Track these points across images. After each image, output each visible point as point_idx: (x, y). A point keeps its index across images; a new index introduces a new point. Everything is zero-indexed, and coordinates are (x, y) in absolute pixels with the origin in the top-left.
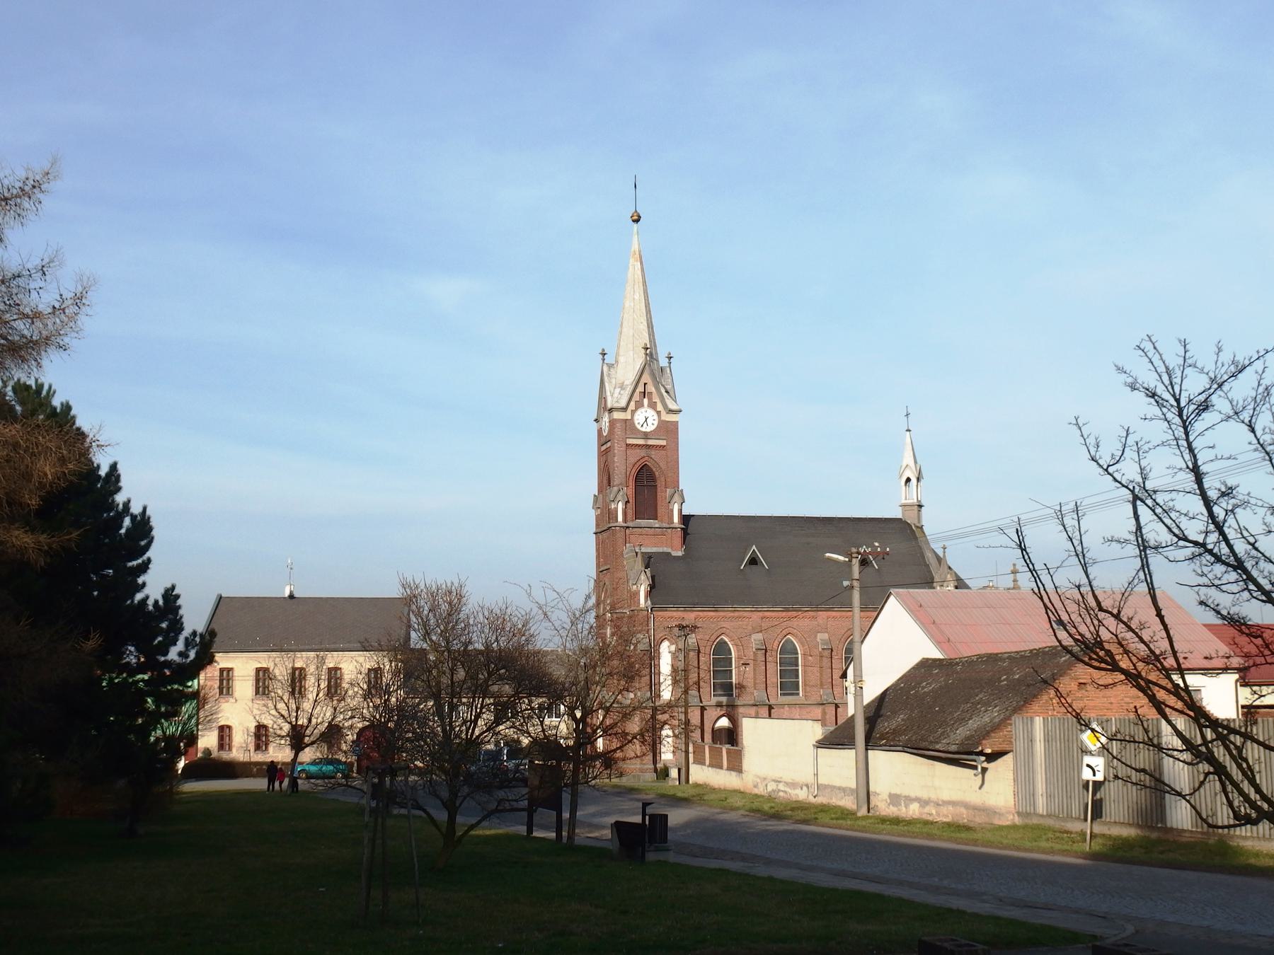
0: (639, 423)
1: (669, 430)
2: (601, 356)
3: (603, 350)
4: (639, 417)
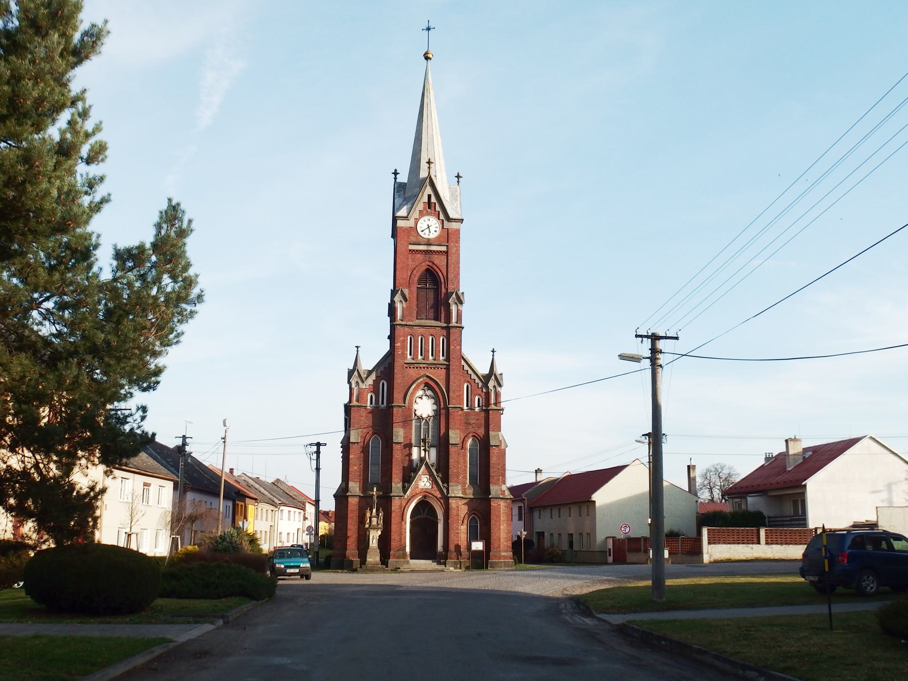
0: (421, 227)
1: (450, 238)
2: (393, 175)
3: (396, 170)
4: (422, 224)
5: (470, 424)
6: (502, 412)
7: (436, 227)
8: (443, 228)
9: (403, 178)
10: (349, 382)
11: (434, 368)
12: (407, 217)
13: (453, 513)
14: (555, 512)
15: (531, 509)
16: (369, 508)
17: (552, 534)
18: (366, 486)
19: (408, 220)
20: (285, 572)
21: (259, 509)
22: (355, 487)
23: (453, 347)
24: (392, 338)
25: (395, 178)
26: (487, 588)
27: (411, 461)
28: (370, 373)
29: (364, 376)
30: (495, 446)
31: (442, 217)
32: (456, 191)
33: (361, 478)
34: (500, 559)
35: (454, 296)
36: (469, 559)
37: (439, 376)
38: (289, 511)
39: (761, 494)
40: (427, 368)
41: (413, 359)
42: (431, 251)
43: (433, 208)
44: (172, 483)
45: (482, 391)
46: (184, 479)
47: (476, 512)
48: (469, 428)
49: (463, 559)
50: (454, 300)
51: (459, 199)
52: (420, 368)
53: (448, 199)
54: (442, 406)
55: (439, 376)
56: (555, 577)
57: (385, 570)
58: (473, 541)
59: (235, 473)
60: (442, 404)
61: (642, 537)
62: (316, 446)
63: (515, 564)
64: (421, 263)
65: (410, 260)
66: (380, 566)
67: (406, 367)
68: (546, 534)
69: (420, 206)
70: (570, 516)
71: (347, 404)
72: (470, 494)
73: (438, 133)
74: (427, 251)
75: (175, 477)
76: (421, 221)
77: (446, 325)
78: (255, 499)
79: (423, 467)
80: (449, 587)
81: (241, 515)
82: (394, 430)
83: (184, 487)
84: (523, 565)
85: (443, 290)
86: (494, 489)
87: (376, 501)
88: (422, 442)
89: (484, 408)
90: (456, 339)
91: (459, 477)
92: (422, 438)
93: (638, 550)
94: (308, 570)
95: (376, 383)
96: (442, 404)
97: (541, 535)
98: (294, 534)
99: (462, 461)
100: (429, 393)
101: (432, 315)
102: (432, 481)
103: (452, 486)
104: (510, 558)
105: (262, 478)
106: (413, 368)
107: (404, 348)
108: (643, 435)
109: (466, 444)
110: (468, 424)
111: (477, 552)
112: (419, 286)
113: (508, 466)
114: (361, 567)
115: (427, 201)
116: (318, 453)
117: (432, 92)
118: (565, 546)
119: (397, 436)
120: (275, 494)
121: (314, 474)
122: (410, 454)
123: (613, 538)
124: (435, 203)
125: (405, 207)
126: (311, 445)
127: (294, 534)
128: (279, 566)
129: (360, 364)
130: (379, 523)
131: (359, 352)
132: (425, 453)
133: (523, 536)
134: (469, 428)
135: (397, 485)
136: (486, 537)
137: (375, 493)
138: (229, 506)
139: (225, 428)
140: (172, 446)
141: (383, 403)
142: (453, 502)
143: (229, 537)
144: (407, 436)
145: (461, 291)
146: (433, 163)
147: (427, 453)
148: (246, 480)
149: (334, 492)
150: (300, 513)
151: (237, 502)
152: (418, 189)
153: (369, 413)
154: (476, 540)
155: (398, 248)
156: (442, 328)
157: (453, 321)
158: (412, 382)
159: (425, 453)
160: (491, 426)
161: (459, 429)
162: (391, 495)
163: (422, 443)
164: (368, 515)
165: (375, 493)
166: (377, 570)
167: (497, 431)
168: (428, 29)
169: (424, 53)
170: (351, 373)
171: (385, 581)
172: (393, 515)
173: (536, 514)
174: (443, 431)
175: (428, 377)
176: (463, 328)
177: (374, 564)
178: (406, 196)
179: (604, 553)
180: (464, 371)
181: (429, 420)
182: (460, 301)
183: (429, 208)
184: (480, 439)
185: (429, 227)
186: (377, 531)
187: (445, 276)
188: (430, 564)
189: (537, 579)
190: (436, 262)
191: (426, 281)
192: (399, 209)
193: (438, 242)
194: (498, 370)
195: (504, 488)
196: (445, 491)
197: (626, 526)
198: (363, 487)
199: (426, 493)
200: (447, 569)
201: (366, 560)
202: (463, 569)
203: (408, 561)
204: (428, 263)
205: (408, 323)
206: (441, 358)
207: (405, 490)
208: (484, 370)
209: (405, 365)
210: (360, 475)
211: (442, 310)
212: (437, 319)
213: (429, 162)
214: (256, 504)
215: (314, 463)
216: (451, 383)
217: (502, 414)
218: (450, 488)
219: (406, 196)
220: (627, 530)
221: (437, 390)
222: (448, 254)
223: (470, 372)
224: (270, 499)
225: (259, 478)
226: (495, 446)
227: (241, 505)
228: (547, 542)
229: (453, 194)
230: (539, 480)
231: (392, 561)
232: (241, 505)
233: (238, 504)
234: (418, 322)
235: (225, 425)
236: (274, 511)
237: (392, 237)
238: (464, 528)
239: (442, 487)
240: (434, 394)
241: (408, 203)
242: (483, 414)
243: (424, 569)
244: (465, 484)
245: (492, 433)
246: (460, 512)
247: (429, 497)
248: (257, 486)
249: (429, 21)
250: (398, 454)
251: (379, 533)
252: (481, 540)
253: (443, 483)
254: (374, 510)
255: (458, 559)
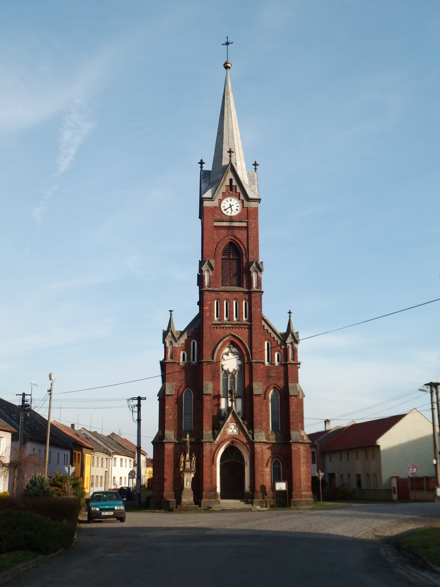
0: (224, 207)
3: (202, 160)
4: (225, 204)
5: (271, 377)
6: (299, 366)
7: (238, 207)
8: (243, 207)
9: (208, 167)
10: (164, 342)
11: (238, 328)
12: (212, 198)
13: (258, 456)
14: (344, 455)
15: (323, 454)
16: (183, 453)
17: (342, 475)
18: (180, 434)
19: (213, 201)
20: (101, 515)
21: (96, 457)
22: (170, 435)
23: (254, 309)
24: (201, 303)
25: (201, 167)
26: (297, 530)
27: (220, 410)
28: (182, 333)
29: (177, 336)
30: (294, 396)
31: (242, 197)
32: (254, 177)
33: (176, 426)
34: (301, 498)
35: (254, 265)
36: (273, 498)
37: (243, 334)
38: (121, 459)
39: (272, 482)
40: (232, 328)
41: (219, 320)
42: (233, 227)
43: (234, 190)
44: (11, 433)
45: (281, 348)
46: (24, 431)
47: (279, 456)
48: (270, 381)
49: (268, 498)
50: (254, 268)
51: (256, 183)
52: (226, 328)
53: (247, 183)
54: (246, 361)
55: (243, 334)
56: (360, 516)
57: (198, 509)
58: (277, 482)
59: (76, 428)
60: (246, 359)
61: (425, 477)
62: (137, 400)
63: (315, 503)
64: (225, 237)
65: (215, 235)
66: (194, 505)
67: (214, 328)
68: (336, 475)
69: (223, 189)
70: (357, 459)
71: (162, 361)
72: (273, 439)
73: (237, 127)
74: (230, 227)
75: (13, 428)
76: (224, 201)
77: (247, 290)
78: (92, 449)
79: (230, 416)
80: (259, 529)
81: (78, 462)
82: (205, 383)
83: (24, 438)
84: (322, 503)
85: (245, 260)
86: (294, 434)
87: (189, 447)
88: (229, 394)
89: (283, 363)
90: (256, 303)
91: (262, 424)
92: (229, 389)
93: (421, 488)
94: (122, 513)
95: (187, 342)
96: (246, 359)
97: (332, 476)
98: (125, 478)
99: (264, 410)
100: (234, 350)
101: (235, 281)
102: (239, 428)
103: (257, 432)
104: (310, 497)
105: (99, 432)
106: (220, 328)
107: (212, 311)
108: (425, 385)
109: (268, 395)
110: (269, 377)
111: (281, 492)
112: (224, 257)
113: (305, 415)
114: (177, 507)
115: (229, 185)
116: (139, 406)
117: (231, 95)
118: (354, 485)
119: (207, 388)
120: (109, 445)
121: (136, 424)
122: (219, 405)
123: (397, 478)
124: (236, 186)
125: (210, 190)
126: (133, 399)
127: (125, 478)
128: (94, 510)
129: (173, 322)
130: (192, 466)
131: (172, 316)
132: (232, 403)
133: (321, 477)
134: (270, 381)
135: (207, 432)
136: (288, 479)
137: (188, 440)
138: (67, 455)
139: (51, 381)
140: (17, 405)
141: (194, 360)
142: (258, 447)
143: (39, 482)
144: (216, 388)
145: (260, 261)
146: (233, 152)
147: (234, 403)
148: (85, 433)
149: (152, 440)
150: (130, 461)
151: (75, 451)
152: (221, 175)
153: (182, 368)
154: (279, 481)
155: (204, 225)
156: (245, 293)
157: (254, 286)
158: (218, 341)
159: (232, 403)
160: (290, 379)
161: (261, 381)
162: (203, 441)
163: (229, 395)
164: (182, 459)
165: (188, 440)
166: (191, 510)
167: (296, 383)
168: (227, 44)
169: (224, 63)
170: (165, 334)
171: (196, 523)
172: (204, 459)
173: (327, 458)
174: (247, 383)
175: (233, 336)
176: (263, 292)
177: (189, 504)
178: (211, 181)
179: (389, 491)
180: (264, 331)
181: (235, 374)
182: (259, 269)
183: (231, 190)
184: (280, 389)
185: (231, 206)
186: (190, 474)
187: (246, 248)
188: (239, 503)
189: (343, 518)
190: (238, 236)
191: (230, 249)
192: (204, 193)
193: (238, 218)
194: (295, 329)
195: (302, 433)
196: (250, 437)
197: (413, 467)
198: (177, 434)
199: (233, 439)
200: (254, 508)
201: (181, 501)
202: (269, 508)
203: (219, 501)
204: (231, 237)
205: (215, 289)
206: (244, 319)
207: (215, 436)
208: (282, 329)
209: (213, 326)
210: (175, 424)
211: (244, 278)
212: (240, 285)
213: (230, 152)
214: (92, 453)
215: (136, 415)
216: (253, 341)
217: (299, 368)
218: (255, 434)
219: (211, 181)
220: (415, 470)
221: (241, 347)
222: (248, 229)
223: (270, 331)
224: (105, 449)
225: (96, 432)
226: (294, 396)
227: (79, 454)
228: (338, 483)
229: (251, 179)
230: (328, 428)
231: (204, 501)
232: (79, 454)
233: (75, 453)
234: (223, 288)
235: (50, 379)
236: (108, 459)
237: (199, 218)
238: (268, 470)
239: (248, 433)
240: (239, 351)
241: (212, 186)
242: (282, 368)
243: (233, 508)
244: (268, 430)
245: (290, 385)
246: (264, 455)
247: (236, 442)
248: (94, 438)
249: (227, 37)
250: (208, 404)
251: (193, 475)
252: (284, 481)
253: (248, 430)
254: (188, 455)
255: (263, 498)
